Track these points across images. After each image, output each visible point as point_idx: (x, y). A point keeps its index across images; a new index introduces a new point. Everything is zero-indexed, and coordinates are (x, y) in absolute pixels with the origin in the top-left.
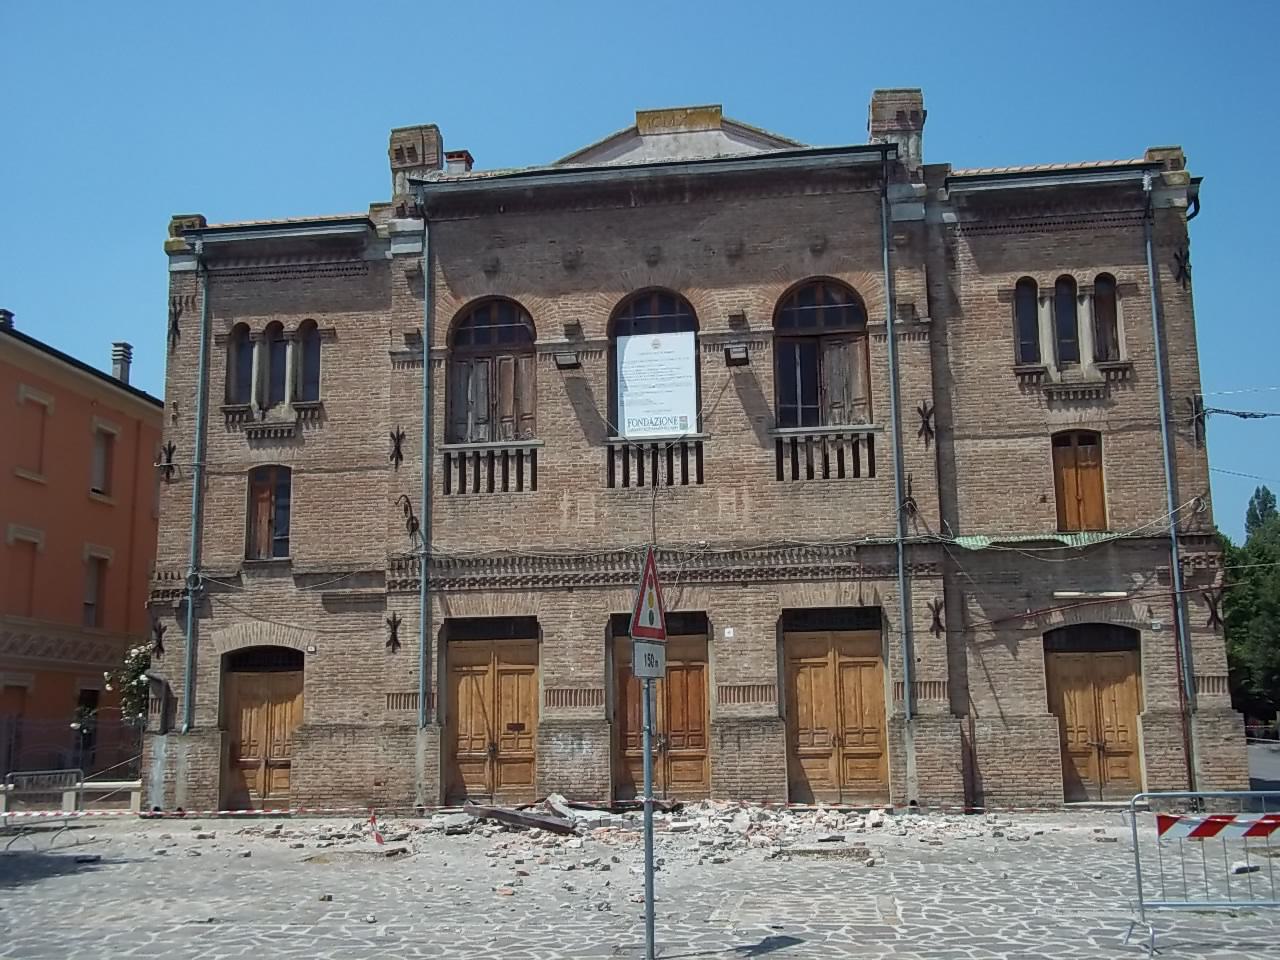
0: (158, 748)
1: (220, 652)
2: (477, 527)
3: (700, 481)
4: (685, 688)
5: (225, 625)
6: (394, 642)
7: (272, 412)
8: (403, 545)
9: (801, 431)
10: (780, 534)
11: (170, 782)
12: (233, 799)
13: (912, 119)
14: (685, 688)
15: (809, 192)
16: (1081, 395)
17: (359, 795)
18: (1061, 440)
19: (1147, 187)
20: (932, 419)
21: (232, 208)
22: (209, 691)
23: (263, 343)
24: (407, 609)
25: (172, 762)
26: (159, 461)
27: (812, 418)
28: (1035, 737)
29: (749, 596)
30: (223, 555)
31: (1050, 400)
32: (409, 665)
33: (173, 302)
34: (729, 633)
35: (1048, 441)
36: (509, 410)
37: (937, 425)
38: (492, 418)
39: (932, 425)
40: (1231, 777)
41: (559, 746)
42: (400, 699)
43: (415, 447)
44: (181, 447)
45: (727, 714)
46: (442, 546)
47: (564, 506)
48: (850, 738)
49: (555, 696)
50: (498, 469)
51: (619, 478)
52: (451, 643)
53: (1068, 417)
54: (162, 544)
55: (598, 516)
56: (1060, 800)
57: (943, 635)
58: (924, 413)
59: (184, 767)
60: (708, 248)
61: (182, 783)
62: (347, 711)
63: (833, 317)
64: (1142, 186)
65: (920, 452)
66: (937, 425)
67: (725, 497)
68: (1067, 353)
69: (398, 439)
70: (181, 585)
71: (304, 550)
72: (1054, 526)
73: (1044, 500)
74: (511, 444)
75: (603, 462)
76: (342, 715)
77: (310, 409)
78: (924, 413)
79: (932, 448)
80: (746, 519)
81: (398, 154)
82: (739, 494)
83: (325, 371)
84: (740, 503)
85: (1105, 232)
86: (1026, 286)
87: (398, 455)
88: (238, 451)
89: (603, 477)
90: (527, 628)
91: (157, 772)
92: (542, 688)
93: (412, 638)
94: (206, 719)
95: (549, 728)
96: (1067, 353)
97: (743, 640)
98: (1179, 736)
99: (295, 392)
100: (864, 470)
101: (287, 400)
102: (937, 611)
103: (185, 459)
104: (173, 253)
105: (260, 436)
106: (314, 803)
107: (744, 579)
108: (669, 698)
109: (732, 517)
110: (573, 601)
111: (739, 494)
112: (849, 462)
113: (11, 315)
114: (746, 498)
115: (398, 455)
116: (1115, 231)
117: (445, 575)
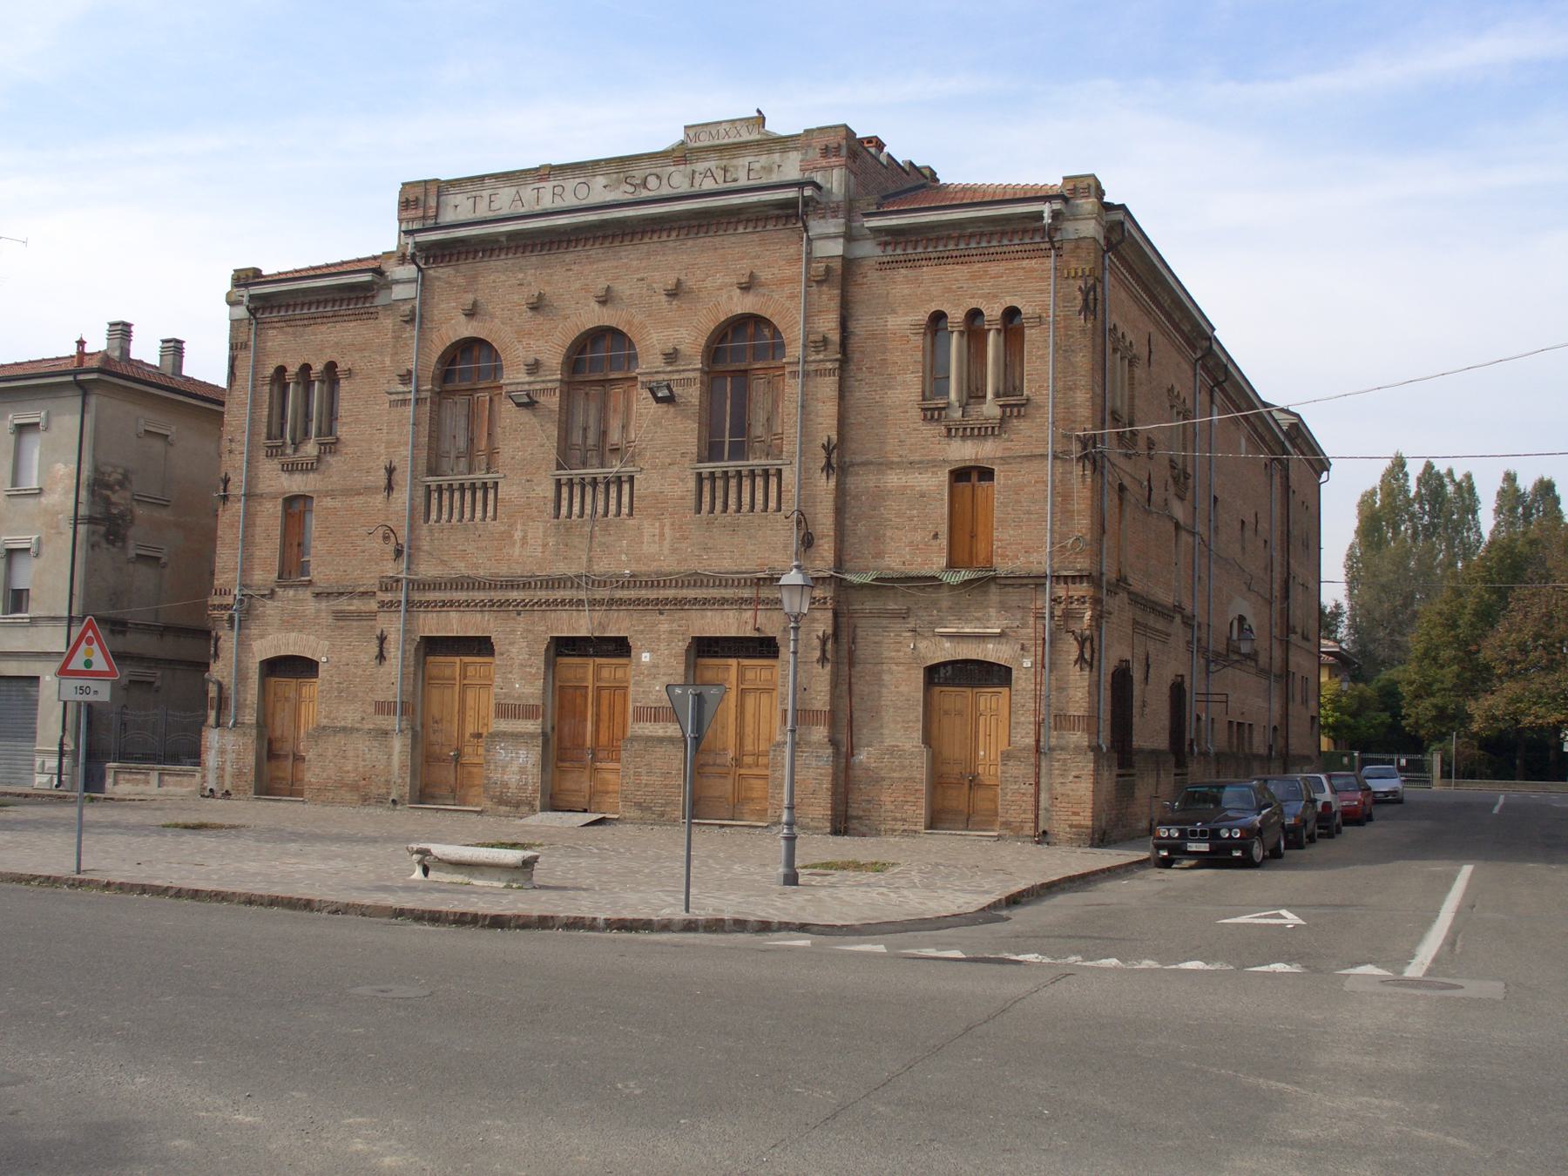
0: (213, 739)
1: (258, 660)
2: (457, 550)
3: (631, 514)
4: (612, 707)
5: (262, 637)
6: (381, 657)
7: (973, 410)
8: (391, 569)
9: (730, 465)
10: (694, 565)
11: (221, 769)
12: (266, 787)
13: (81, 343)
14: (612, 707)
15: (741, 230)
16: (981, 432)
17: (354, 788)
18: (960, 475)
19: (1047, 220)
20: (834, 455)
21: (279, 258)
22: (252, 693)
23: (322, 382)
24: (393, 624)
25: (222, 752)
26: (217, 490)
27: (738, 452)
28: (904, 767)
29: (664, 624)
30: (264, 575)
31: (949, 434)
32: (392, 677)
33: (231, 348)
34: (646, 657)
35: (944, 477)
36: (483, 444)
37: (838, 460)
38: (470, 451)
39: (834, 461)
40: (1075, 814)
41: (501, 753)
42: (382, 708)
43: (403, 478)
44: (234, 478)
45: (640, 732)
46: (427, 570)
47: (518, 535)
48: (748, 760)
49: (504, 711)
50: (468, 495)
51: (564, 511)
52: (431, 659)
53: (965, 452)
54: (219, 564)
55: (545, 545)
56: (921, 828)
57: (828, 667)
58: (828, 449)
59: (230, 757)
60: (650, 288)
61: (229, 769)
62: (349, 715)
63: (759, 353)
64: (1042, 218)
65: (825, 486)
66: (838, 460)
67: (649, 529)
68: (974, 394)
69: (390, 471)
70: (229, 600)
71: (321, 571)
72: (944, 562)
73: (936, 536)
74: (480, 476)
75: (551, 494)
76: (345, 719)
77: (330, 446)
78: (828, 449)
79: (832, 483)
80: (666, 552)
81: (405, 204)
82: (662, 527)
83: (344, 407)
84: (662, 535)
85: (1016, 264)
86: (938, 318)
87: (390, 487)
88: (277, 481)
89: (551, 506)
90: (481, 646)
91: (211, 759)
92: (493, 702)
93: (394, 651)
94: (250, 718)
95: (494, 736)
96: (974, 394)
97: (655, 663)
98: (1031, 771)
99: (319, 428)
100: (772, 504)
101: (990, 396)
102: (824, 642)
103: (237, 488)
104: (232, 302)
105: (290, 468)
106: (324, 793)
107: (660, 605)
108: (598, 715)
109: (655, 548)
110: (521, 623)
111: (662, 527)
112: (759, 496)
113: (181, 342)
114: (667, 530)
115: (390, 487)
116: (1025, 263)
117: (415, 594)
